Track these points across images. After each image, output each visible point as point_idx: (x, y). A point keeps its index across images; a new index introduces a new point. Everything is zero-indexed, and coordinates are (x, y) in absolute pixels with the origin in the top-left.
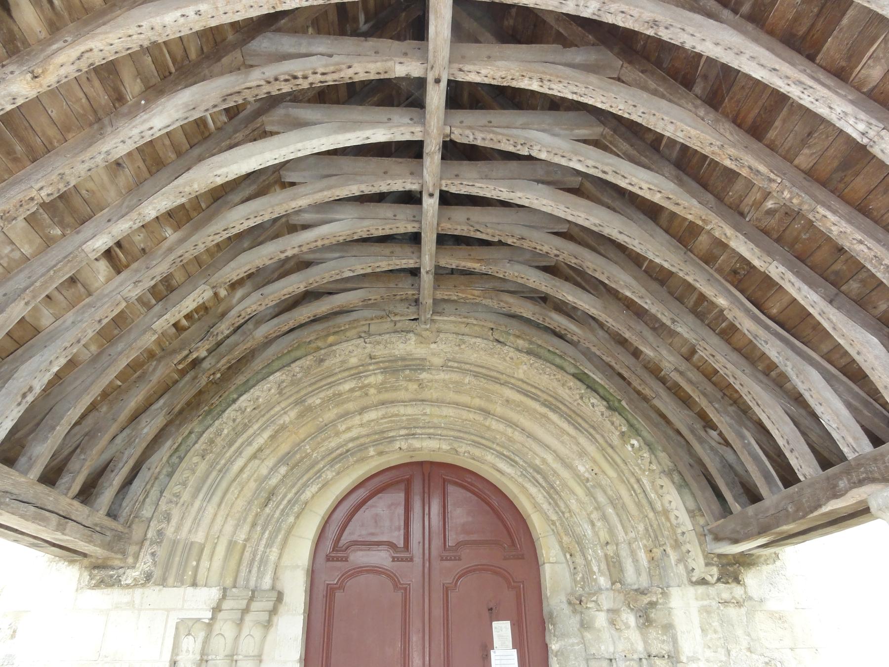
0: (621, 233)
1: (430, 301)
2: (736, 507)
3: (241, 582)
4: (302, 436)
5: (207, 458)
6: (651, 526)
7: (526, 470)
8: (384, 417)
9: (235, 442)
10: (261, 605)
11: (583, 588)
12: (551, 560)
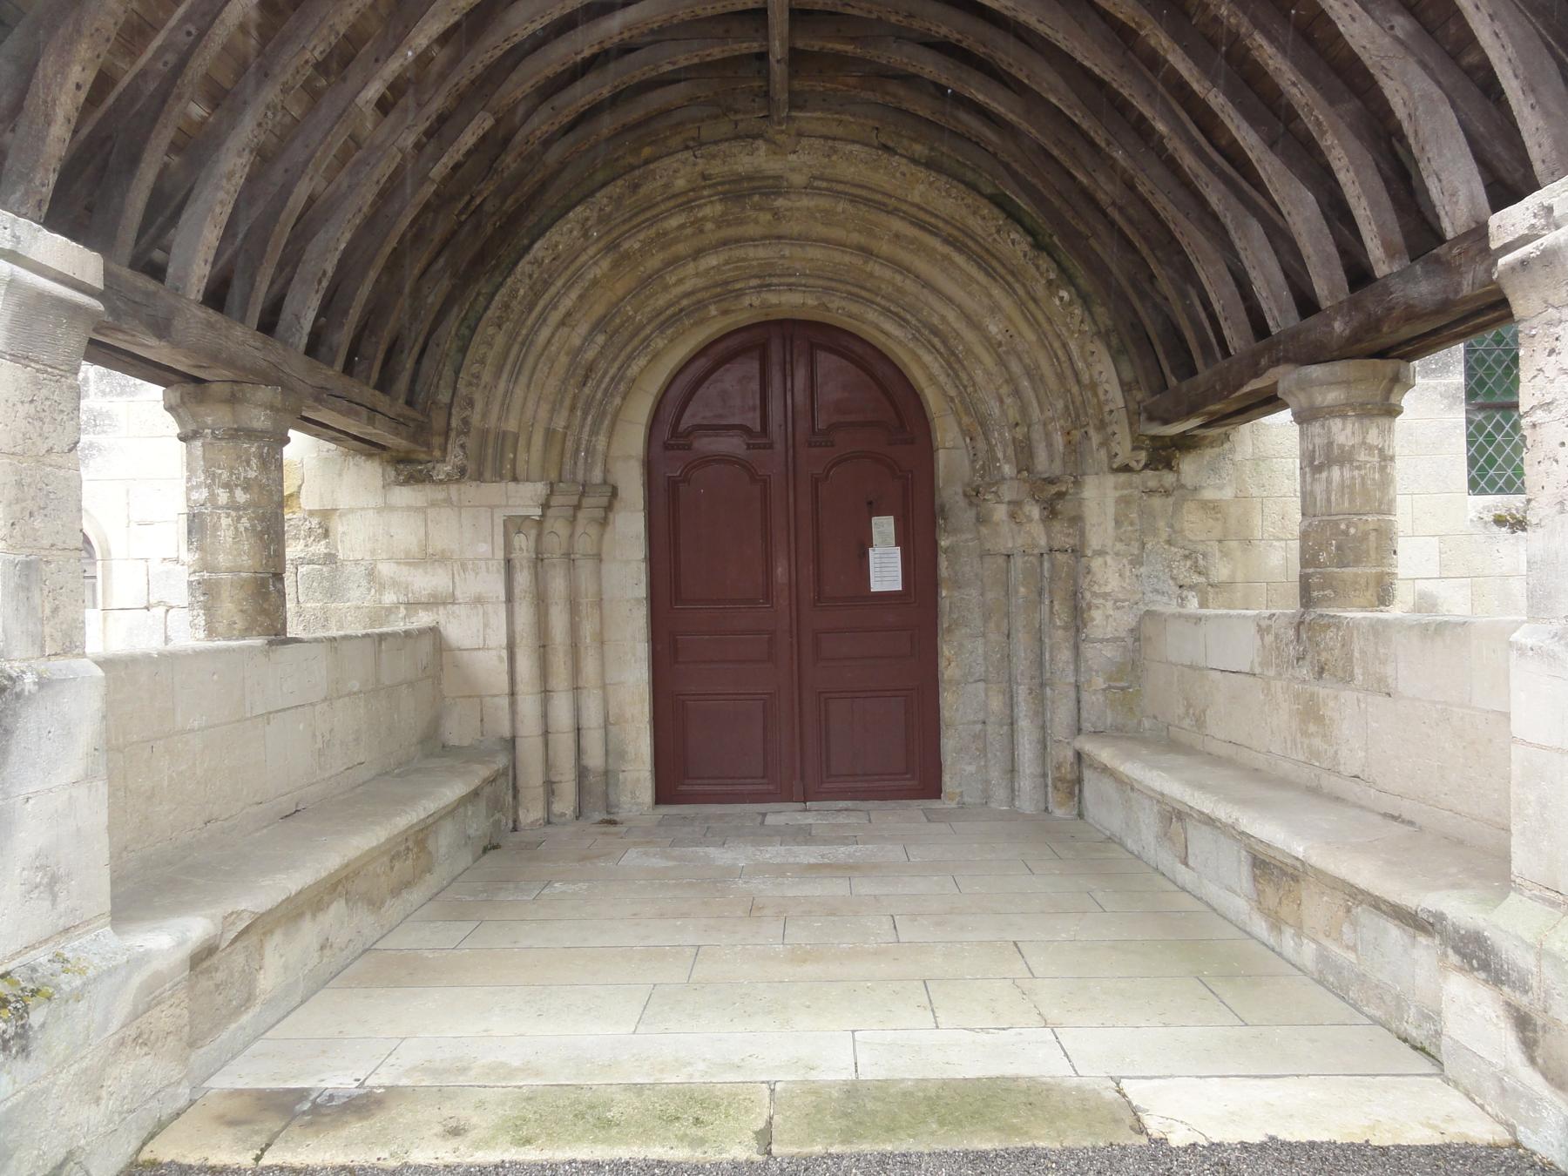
0: (1039, 21)
1: (785, 96)
2: (1173, 381)
3: (567, 475)
4: (620, 293)
5: (504, 327)
6: (1073, 403)
7: (919, 331)
8: (727, 263)
9: (536, 304)
10: (594, 501)
11: (982, 477)
12: (947, 445)
